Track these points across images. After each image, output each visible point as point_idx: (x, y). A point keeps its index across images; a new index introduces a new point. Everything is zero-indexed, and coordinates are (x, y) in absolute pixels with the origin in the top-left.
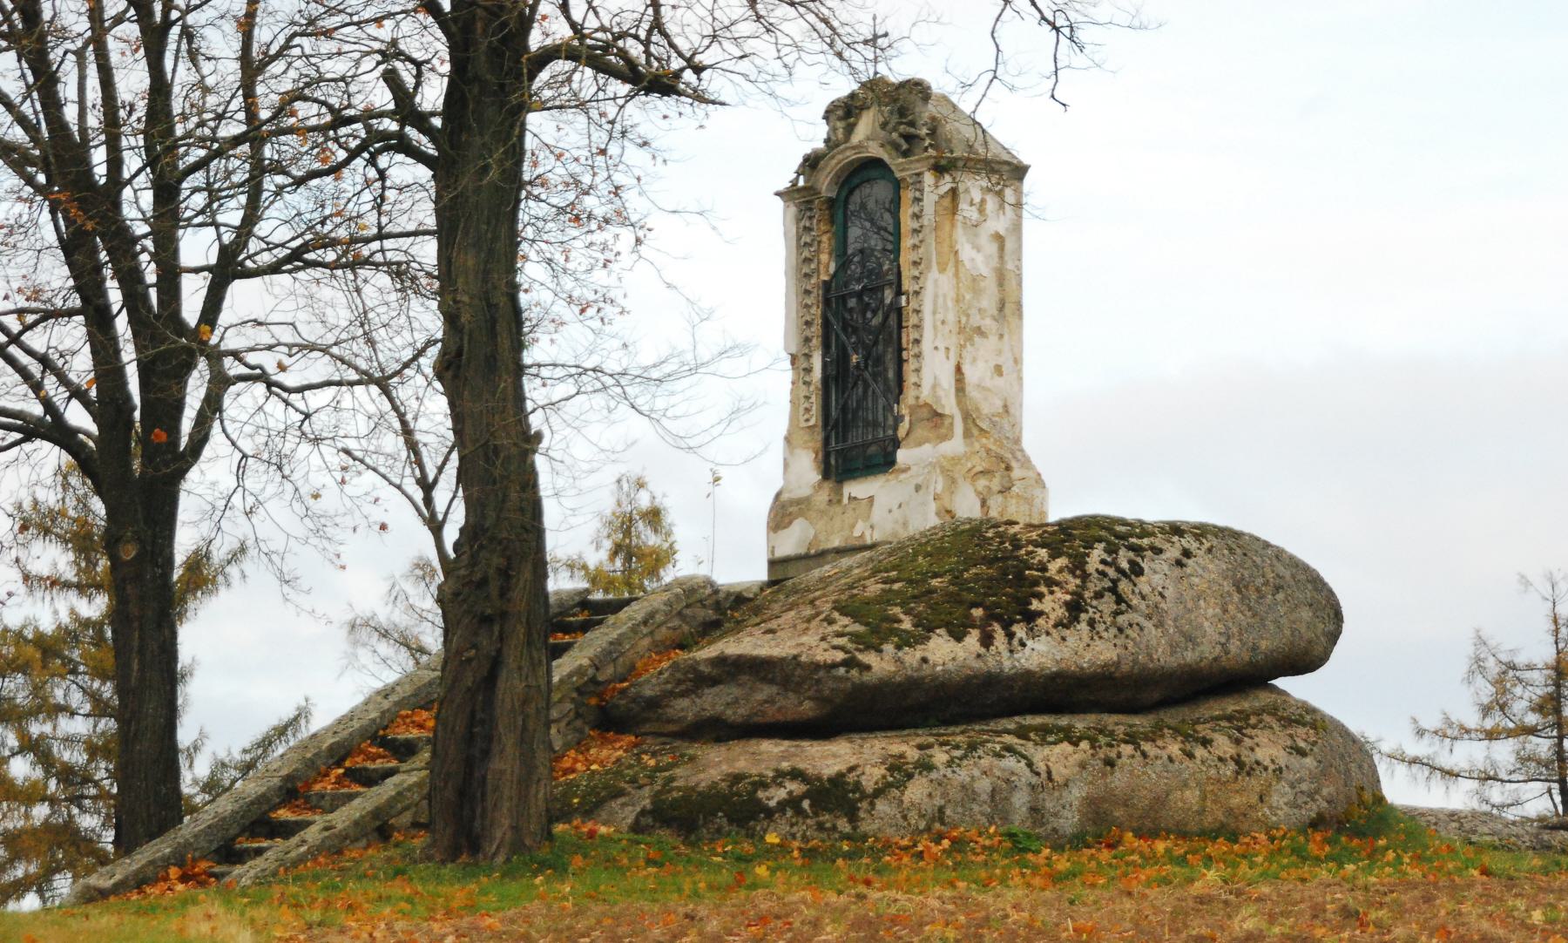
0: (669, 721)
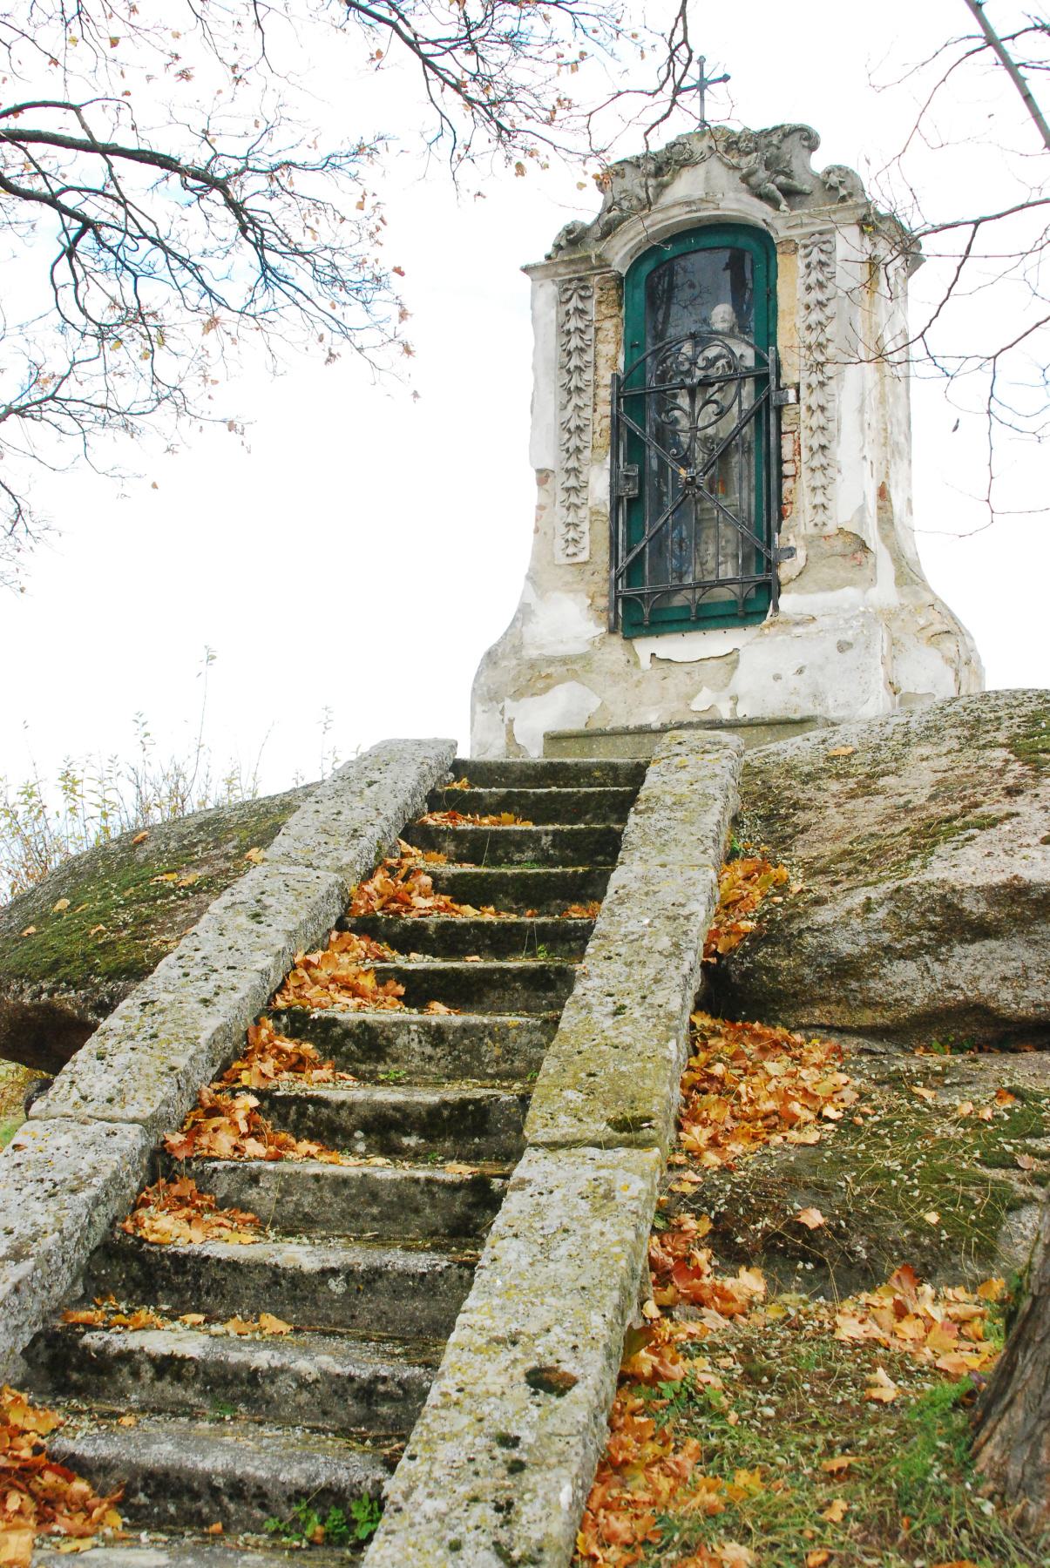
0: (868, 1004)
